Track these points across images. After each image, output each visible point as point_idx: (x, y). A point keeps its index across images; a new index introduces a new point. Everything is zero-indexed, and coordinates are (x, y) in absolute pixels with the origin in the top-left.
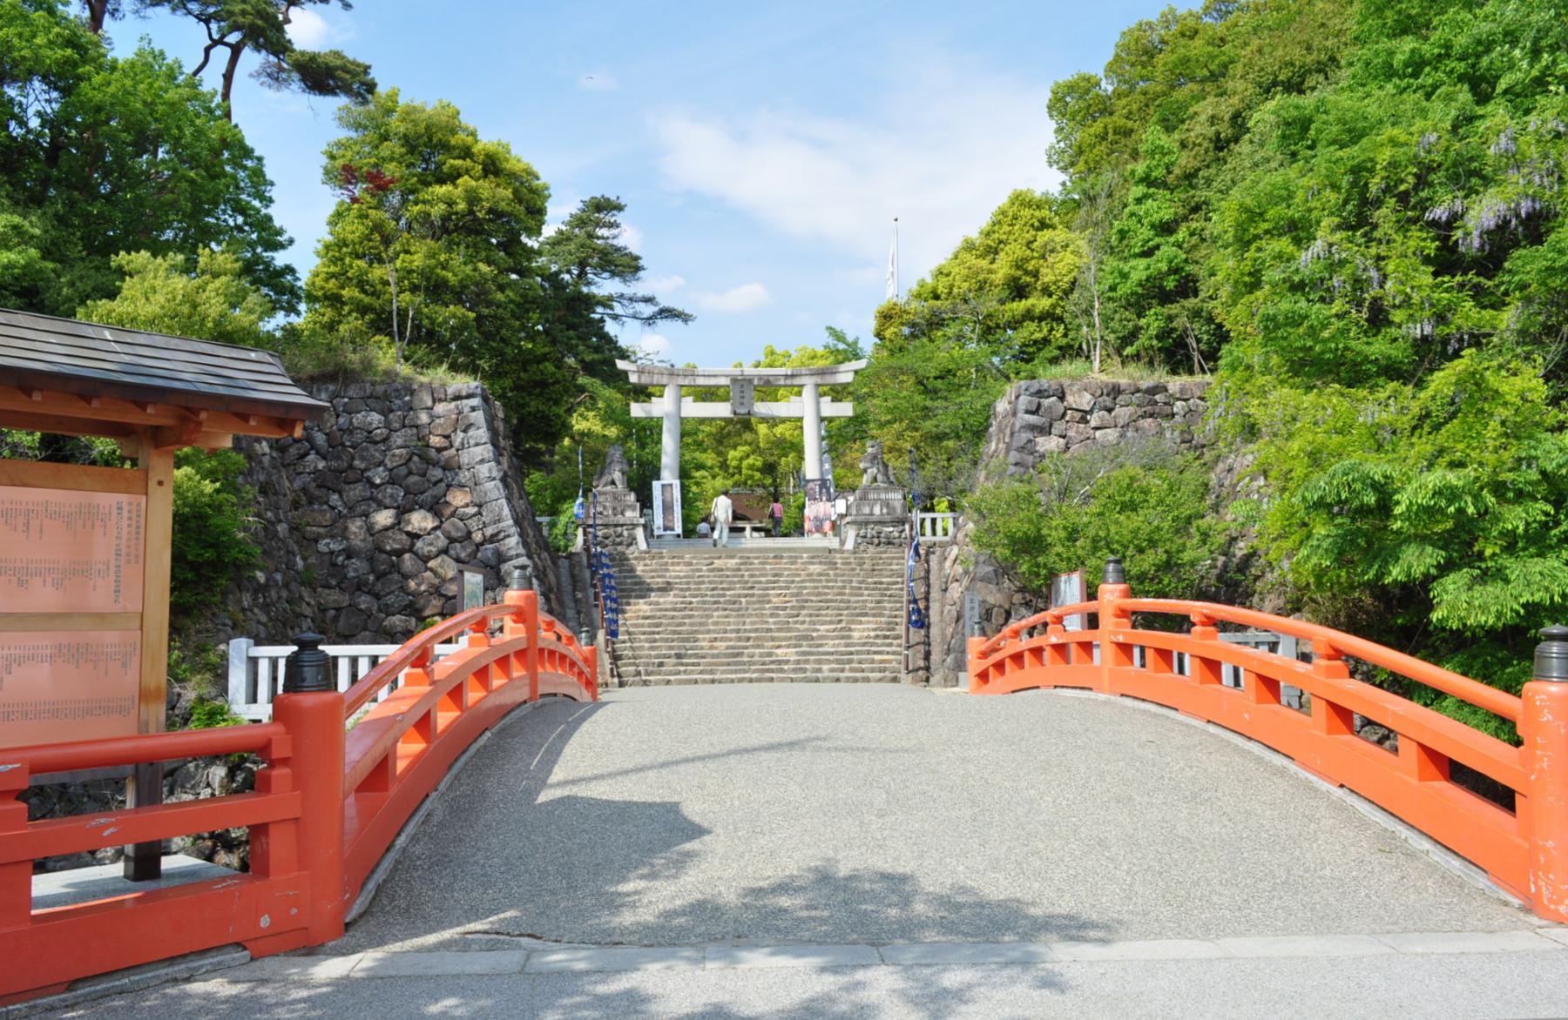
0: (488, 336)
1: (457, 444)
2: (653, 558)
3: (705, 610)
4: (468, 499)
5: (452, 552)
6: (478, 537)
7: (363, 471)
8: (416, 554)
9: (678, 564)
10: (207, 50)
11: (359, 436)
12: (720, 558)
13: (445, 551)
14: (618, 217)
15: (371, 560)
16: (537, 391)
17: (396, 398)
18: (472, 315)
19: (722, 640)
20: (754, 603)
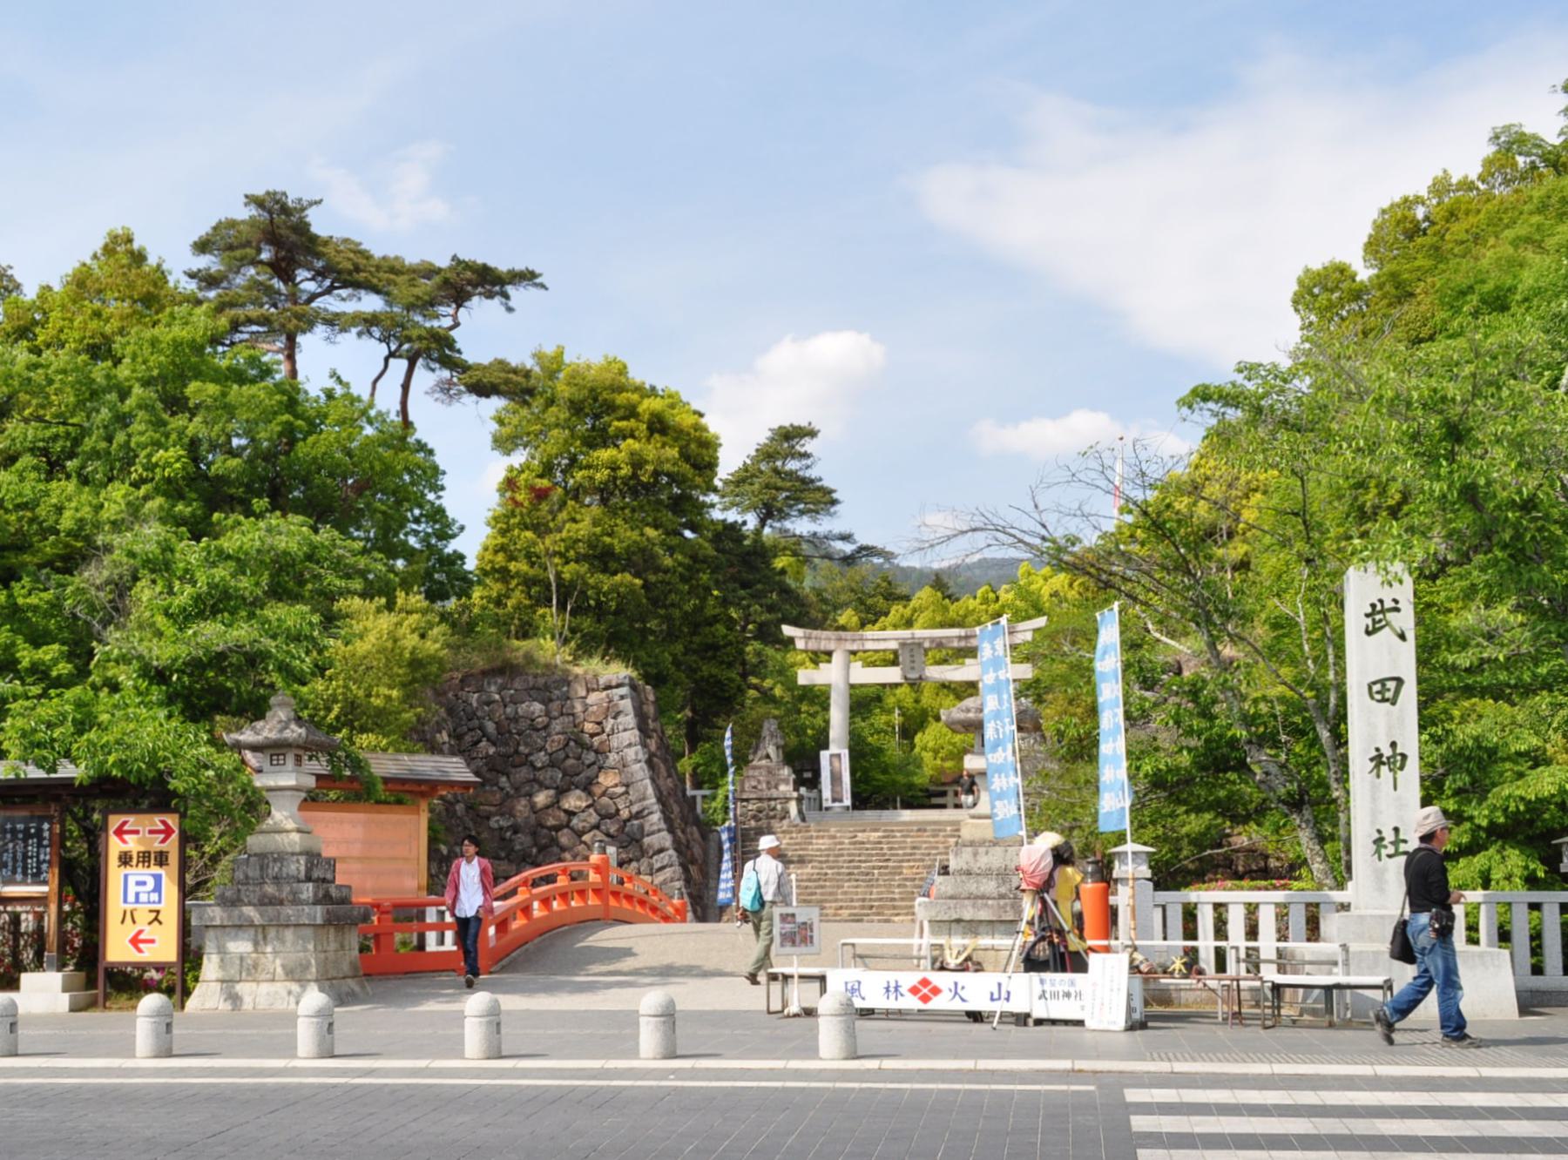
0: (655, 602)
1: (608, 730)
2: (800, 832)
3: (838, 881)
4: (617, 781)
5: (603, 827)
6: (625, 814)
7: (527, 756)
8: (572, 829)
9: (823, 837)
10: (386, 360)
11: (523, 724)
12: (864, 831)
13: (597, 827)
14: (808, 445)
15: (534, 834)
16: (710, 654)
17: (556, 688)
18: (638, 582)
19: (847, 908)
20: (886, 874)
